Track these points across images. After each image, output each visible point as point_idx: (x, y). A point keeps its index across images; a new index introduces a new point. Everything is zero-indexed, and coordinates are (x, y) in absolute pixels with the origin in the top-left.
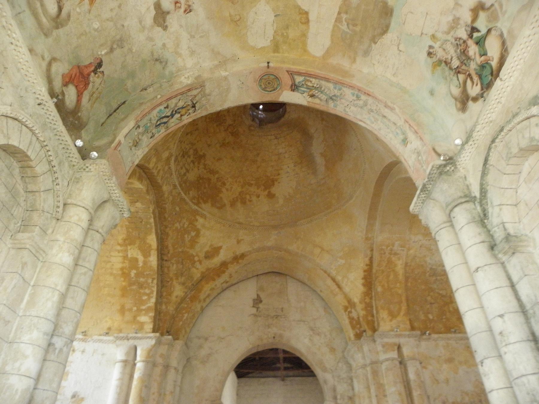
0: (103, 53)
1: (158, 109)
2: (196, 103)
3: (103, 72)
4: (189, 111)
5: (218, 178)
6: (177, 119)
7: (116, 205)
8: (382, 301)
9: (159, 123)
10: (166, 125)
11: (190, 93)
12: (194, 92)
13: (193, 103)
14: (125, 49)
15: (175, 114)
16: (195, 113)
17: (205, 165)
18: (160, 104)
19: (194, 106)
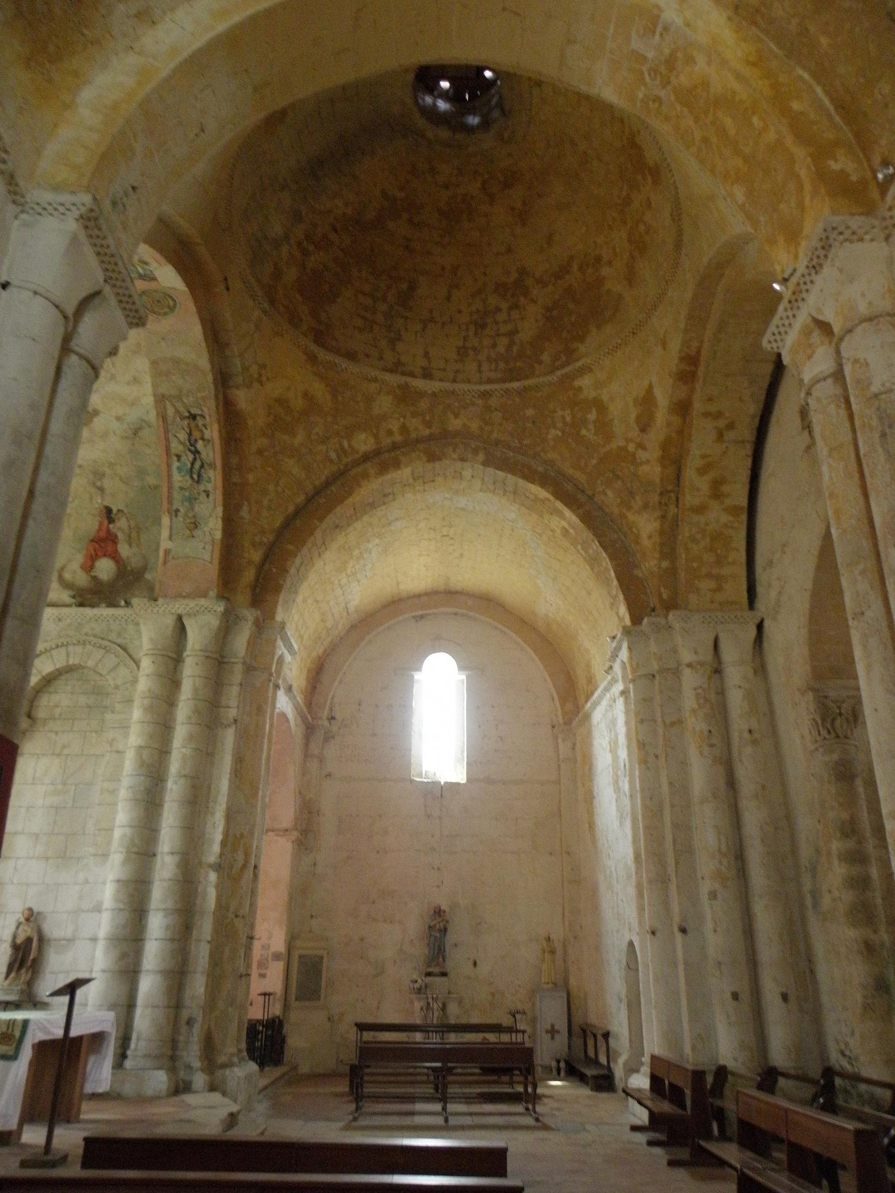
0: (99, 501)
1: (175, 472)
2: (189, 412)
3: (119, 510)
4: (200, 425)
5: (580, 268)
6: (205, 446)
7: (192, 615)
8: (762, 219)
9: (195, 477)
10: (206, 466)
11: (170, 420)
12: (170, 411)
13: (188, 417)
14: (108, 471)
15: (196, 447)
16: (207, 417)
17: (540, 282)
18: (169, 466)
19: (193, 417)
